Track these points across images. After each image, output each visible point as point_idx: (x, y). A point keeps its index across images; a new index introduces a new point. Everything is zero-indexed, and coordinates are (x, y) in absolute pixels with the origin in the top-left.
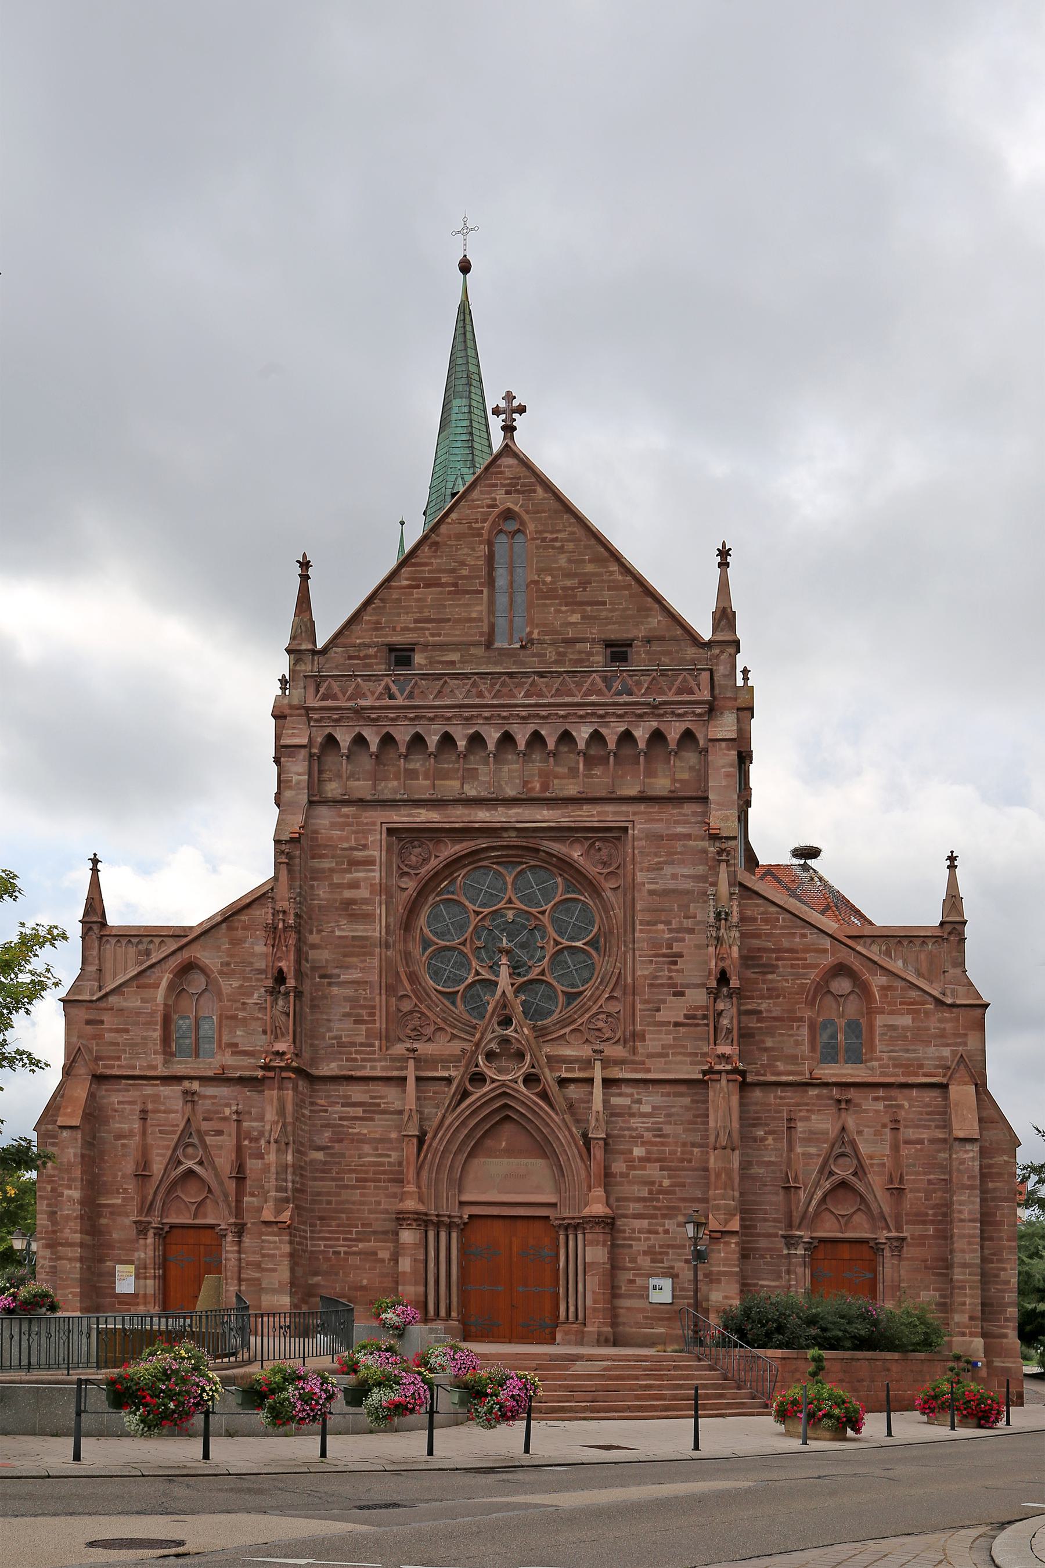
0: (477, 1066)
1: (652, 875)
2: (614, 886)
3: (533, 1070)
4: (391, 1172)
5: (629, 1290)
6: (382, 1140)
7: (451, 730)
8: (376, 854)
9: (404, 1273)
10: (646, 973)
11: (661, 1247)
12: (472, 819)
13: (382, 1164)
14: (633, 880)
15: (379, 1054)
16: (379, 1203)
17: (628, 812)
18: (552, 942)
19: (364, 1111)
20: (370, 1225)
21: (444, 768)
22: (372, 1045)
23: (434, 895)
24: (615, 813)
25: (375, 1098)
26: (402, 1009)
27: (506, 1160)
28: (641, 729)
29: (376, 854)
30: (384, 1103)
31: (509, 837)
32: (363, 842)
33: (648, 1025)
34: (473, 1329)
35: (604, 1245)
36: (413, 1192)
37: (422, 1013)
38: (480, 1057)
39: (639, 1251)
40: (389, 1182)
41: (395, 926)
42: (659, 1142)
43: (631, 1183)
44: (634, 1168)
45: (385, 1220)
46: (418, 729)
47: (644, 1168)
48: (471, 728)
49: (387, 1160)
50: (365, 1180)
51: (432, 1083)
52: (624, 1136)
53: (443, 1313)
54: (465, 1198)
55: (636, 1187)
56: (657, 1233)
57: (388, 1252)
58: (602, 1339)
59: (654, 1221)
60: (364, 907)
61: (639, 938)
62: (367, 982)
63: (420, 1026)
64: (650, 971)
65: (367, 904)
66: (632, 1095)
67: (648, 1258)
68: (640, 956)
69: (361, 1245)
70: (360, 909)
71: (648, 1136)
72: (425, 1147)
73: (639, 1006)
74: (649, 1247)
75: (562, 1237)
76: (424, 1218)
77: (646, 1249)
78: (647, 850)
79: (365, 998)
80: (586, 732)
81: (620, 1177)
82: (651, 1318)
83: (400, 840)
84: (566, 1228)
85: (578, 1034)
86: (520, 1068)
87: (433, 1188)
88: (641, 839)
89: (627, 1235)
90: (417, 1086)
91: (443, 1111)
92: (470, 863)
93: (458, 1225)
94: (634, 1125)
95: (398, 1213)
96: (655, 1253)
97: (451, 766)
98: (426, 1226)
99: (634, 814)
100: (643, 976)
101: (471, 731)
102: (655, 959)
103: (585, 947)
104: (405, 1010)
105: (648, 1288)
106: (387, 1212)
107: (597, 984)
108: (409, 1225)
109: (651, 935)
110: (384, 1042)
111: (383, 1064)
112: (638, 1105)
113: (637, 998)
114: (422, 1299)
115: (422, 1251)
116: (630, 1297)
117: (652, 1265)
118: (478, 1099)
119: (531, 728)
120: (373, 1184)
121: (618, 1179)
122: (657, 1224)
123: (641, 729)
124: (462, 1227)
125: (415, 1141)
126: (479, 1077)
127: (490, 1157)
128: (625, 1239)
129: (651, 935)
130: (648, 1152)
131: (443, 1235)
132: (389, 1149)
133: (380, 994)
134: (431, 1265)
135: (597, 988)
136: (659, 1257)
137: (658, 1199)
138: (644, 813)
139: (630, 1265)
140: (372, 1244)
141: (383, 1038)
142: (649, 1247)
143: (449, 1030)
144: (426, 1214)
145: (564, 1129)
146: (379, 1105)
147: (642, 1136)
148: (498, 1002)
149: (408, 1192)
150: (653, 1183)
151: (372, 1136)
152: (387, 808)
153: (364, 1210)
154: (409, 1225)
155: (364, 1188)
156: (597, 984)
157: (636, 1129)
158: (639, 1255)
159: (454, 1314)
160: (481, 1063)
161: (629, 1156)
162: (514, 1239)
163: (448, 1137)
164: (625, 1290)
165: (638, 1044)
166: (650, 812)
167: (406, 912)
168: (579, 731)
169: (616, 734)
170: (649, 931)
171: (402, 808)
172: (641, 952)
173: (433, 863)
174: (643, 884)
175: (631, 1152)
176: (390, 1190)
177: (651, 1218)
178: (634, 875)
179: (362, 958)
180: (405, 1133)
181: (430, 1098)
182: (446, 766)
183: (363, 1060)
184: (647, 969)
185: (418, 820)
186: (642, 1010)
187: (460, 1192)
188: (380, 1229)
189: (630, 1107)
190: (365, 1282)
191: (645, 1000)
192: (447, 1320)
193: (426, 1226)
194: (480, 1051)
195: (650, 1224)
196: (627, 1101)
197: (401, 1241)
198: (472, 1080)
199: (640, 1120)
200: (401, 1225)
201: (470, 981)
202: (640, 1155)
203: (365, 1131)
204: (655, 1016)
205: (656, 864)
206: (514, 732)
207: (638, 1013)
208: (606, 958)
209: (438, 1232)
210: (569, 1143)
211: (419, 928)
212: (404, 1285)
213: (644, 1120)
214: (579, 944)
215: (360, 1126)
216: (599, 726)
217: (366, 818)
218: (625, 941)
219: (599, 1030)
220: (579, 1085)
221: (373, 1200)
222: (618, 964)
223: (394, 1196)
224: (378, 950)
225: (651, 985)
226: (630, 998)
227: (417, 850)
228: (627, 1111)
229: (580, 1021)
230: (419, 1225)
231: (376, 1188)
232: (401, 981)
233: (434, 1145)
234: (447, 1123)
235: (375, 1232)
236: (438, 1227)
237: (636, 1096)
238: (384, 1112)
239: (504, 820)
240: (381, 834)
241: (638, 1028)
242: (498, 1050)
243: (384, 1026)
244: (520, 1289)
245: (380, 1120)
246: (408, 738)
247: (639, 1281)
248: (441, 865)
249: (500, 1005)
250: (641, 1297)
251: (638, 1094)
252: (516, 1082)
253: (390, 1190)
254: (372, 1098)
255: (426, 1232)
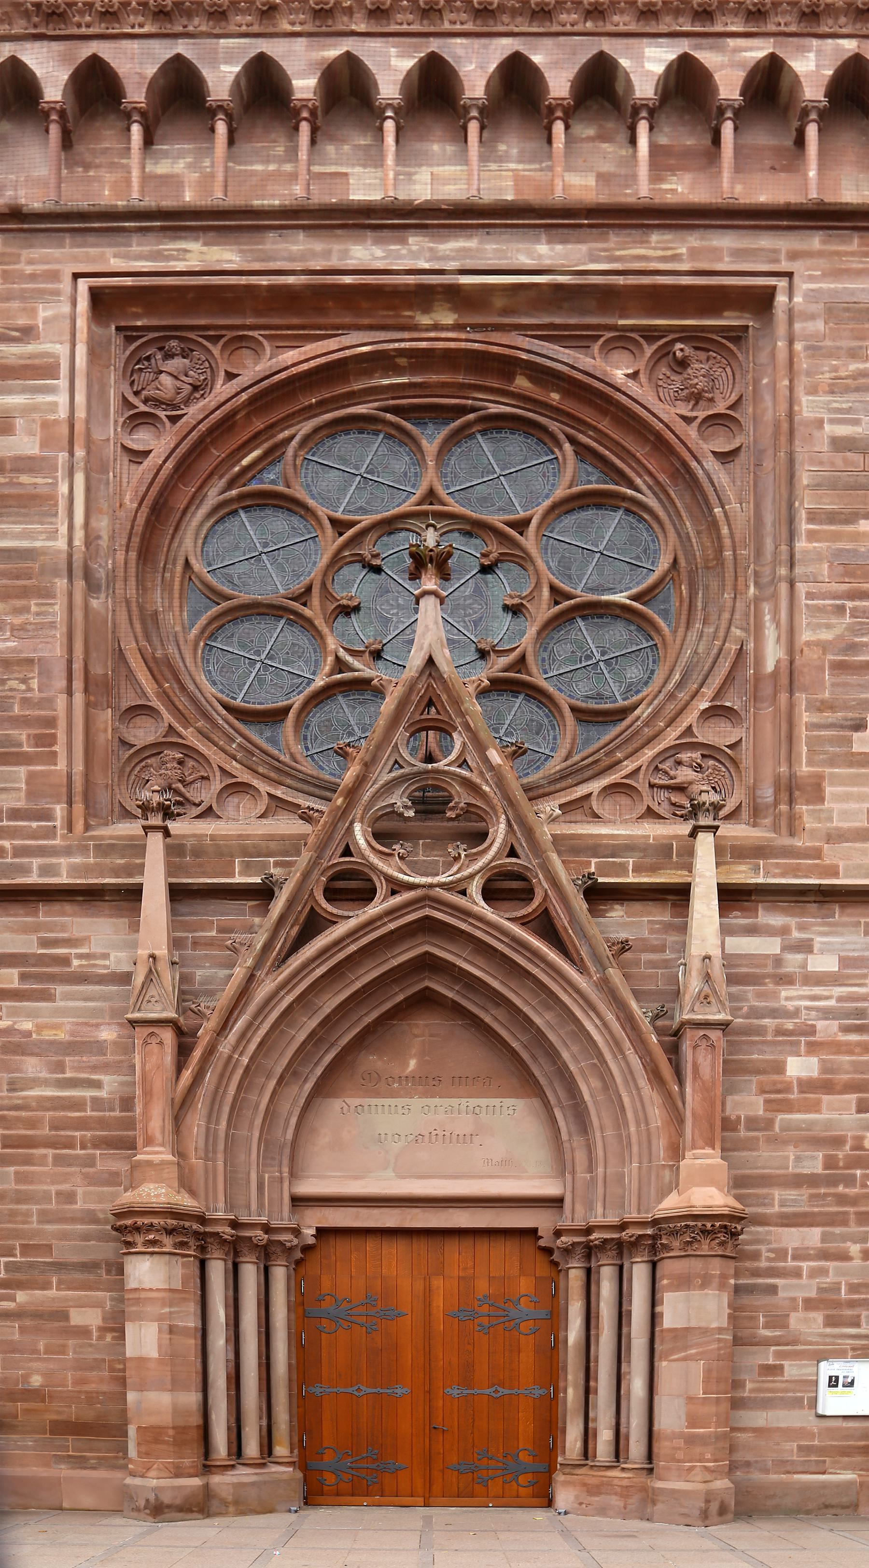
0: (347, 852)
1: (841, 402)
2: (727, 449)
3: (514, 860)
4: (102, 1123)
5: (760, 1390)
6: (73, 1047)
7: (274, 48)
8: (61, 350)
9: (141, 1361)
10: (826, 635)
11: (853, 1288)
12: (335, 262)
13: (77, 1104)
14: (791, 415)
15: (63, 837)
16: (70, 1197)
17: (776, 251)
18: (546, 592)
19: (23, 977)
20: (48, 1249)
21: (253, 173)
22: (46, 815)
23: (223, 482)
24: (737, 254)
25: (55, 943)
26: (131, 740)
27: (417, 1103)
28: (812, 55)
29: (61, 350)
30: (80, 956)
31: (436, 327)
32: (21, 322)
33: (832, 762)
34: (330, 1479)
35: (722, 1287)
36: (163, 1163)
37: (189, 752)
38: (357, 827)
39: (794, 1300)
40: (95, 1146)
41: (112, 538)
42: (859, 1044)
43: (775, 1141)
44: (788, 1107)
45: (86, 1237)
46: (183, 48)
47: (815, 1107)
48: (334, 46)
49: (88, 1093)
50: (30, 1143)
51: (215, 905)
52: (760, 1031)
53: (252, 1448)
54: (306, 1188)
55: (791, 1153)
56: (845, 1257)
57: (99, 1310)
58: (714, 1507)
59: (838, 1230)
60: (24, 479)
61: (806, 552)
62: (30, 661)
63: (182, 781)
64: (838, 631)
65: (31, 470)
66: (784, 931)
67: (818, 1317)
68: (810, 596)
69: (21, 1296)
70: (11, 484)
71: (827, 1029)
72: (197, 1054)
73: (805, 717)
74: (820, 1290)
75: (575, 1277)
76: (196, 1226)
77: (813, 1294)
78: (828, 343)
79: (25, 701)
80: (660, 61)
81: (748, 1129)
82: (821, 1451)
83: (129, 334)
84: (589, 1251)
85: (624, 800)
86: (472, 858)
87: (220, 1156)
88: (812, 317)
89: (764, 1264)
90: (173, 912)
91: (250, 962)
92: (324, 405)
93: (289, 1251)
94: (790, 1005)
95: (119, 1215)
96: (838, 1304)
97: (272, 167)
98: (203, 1249)
99: (794, 256)
100: (818, 643)
101: (333, 53)
102: (849, 604)
103: (635, 604)
104: (140, 743)
105: (816, 1383)
106: (91, 1217)
107: (671, 686)
108: (153, 1243)
109: (840, 545)
110: (79, 807)
111: (77, 860)
112: (799, 957)
113: (801, 698)
114: (196, 1420)
115: (192, 1308)
116: (766, 1404)
117: (828, 1330)
118: (352, 934)
119: (503, 47)
120: (50, 1152)
121: (743, 1133)
122: (844, 1238)
123: (812, 55)
124: (298, 1255)
125: (168, 1036)
126: (353, 884)
127: (377, 1094)
128: (756, 1273)
129: (840, 545)
130: (826, 1068)
131: (250, 1274)
132: (94, 1068)
133: (70, 692)
134: (219, 1341)
135: (672, 696)
136: (849, 1312)
137: (850, 1181)
138: (820, 254)
139: (767, 1333)
140: (53, 1293)
141: (78, 798)
142: (820, 1290)
143: (264, 787)
144: (202, 1219)
145: (602, 1007)
146: (65, 961)
147: (812, 1030)
148: (412, 687)
149: (149, 1163)
150: (838, 1142)
151: (48, 1035)
152: (91, 239)
153: (28, 1214)
154: (153, 1243)
155: (28, 1161)
156: (671, 686)
157: (796, 1013)
158: (795, 1309)
159: (281, 1450)
160: (362, 842)
161: (775, 1077)
162: (438, 1283)
163: (262, 1032)
164: (751, 1391)
165: (803, 808)
166: (838, 254)
167: (145, 510)
168: (639, 58)
169: (741, 65)
170: (836, 537)
171: (135, 238)
172: (813, 588)
173: (222, 390)
174: (820, 423)
175: (780, 1068)
176: (99, 1166)
177: (832, 1224)
178: (792, 401)
179: (19, 603)
180: (137, 1015)
181: (210, 943)
182: (259, 167)
183: (19, 852)
184: (828, 626)
185: (180, 266)
186: (812, 726)
187: (293, 1175)
188: (74, 1258)
189: (778, 961)
190: (36, 1381)
191: (823, 702)
192: (263, 1465)
193: (203, 1249)
194: (358, 811)
195: (825, 1238)
196: (771, 946)
197: (131, 1284)
198: (332, 894)
199: (806, 991)
200: (129, 1244)
201: (320, 682)
202: (804, 1074)
203: (27, 1025)
204: (850, 741)
205: (854, 377)
206: (458, 58)
207: (803, 733)
208: (698, 625)
209: (236, 1266)
210: (617, 1043)
211: (180, 562)
212: (141, 1389)
213: (818, 990)
214: (620, 598)
215: (13, 1013)
216: (697, 47)
217: (31, 262)
218: (756, 574)
219: (680, 789)
220: (637, 906)
221: (53, 1188)
222: (736, 632)
223: (113, 1179)
224: (61, 583)
225: (839, 667)
226: (783, 697)
227: (176, 364)
228: (769, 970)
229: (629, 766)
230: (183, 1245)
231: (59, 1161)
232: (130, 675)
233: (225, 1048)
234: (262, 992)
235: (60, 1266)
236: (237, 1254)
237: (796, 934)
238: (82, 978)
239: (426, 266)
240: (74, 303)
241: (804, 769)
242: (411, 813)
243: (79, 768)
244: (455, 1392)
245: (67, 997)
246: (151, 70)
247: (792, 1370)
248: (244, 396)
249: (415, 698)
250: (797, 1403)
251: (801, 928)
252: (464, 893)
253: (99, 1166)
254: (45, 943)
255: (203, 1264)
